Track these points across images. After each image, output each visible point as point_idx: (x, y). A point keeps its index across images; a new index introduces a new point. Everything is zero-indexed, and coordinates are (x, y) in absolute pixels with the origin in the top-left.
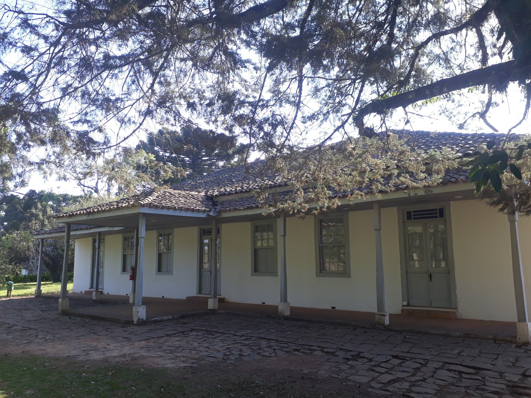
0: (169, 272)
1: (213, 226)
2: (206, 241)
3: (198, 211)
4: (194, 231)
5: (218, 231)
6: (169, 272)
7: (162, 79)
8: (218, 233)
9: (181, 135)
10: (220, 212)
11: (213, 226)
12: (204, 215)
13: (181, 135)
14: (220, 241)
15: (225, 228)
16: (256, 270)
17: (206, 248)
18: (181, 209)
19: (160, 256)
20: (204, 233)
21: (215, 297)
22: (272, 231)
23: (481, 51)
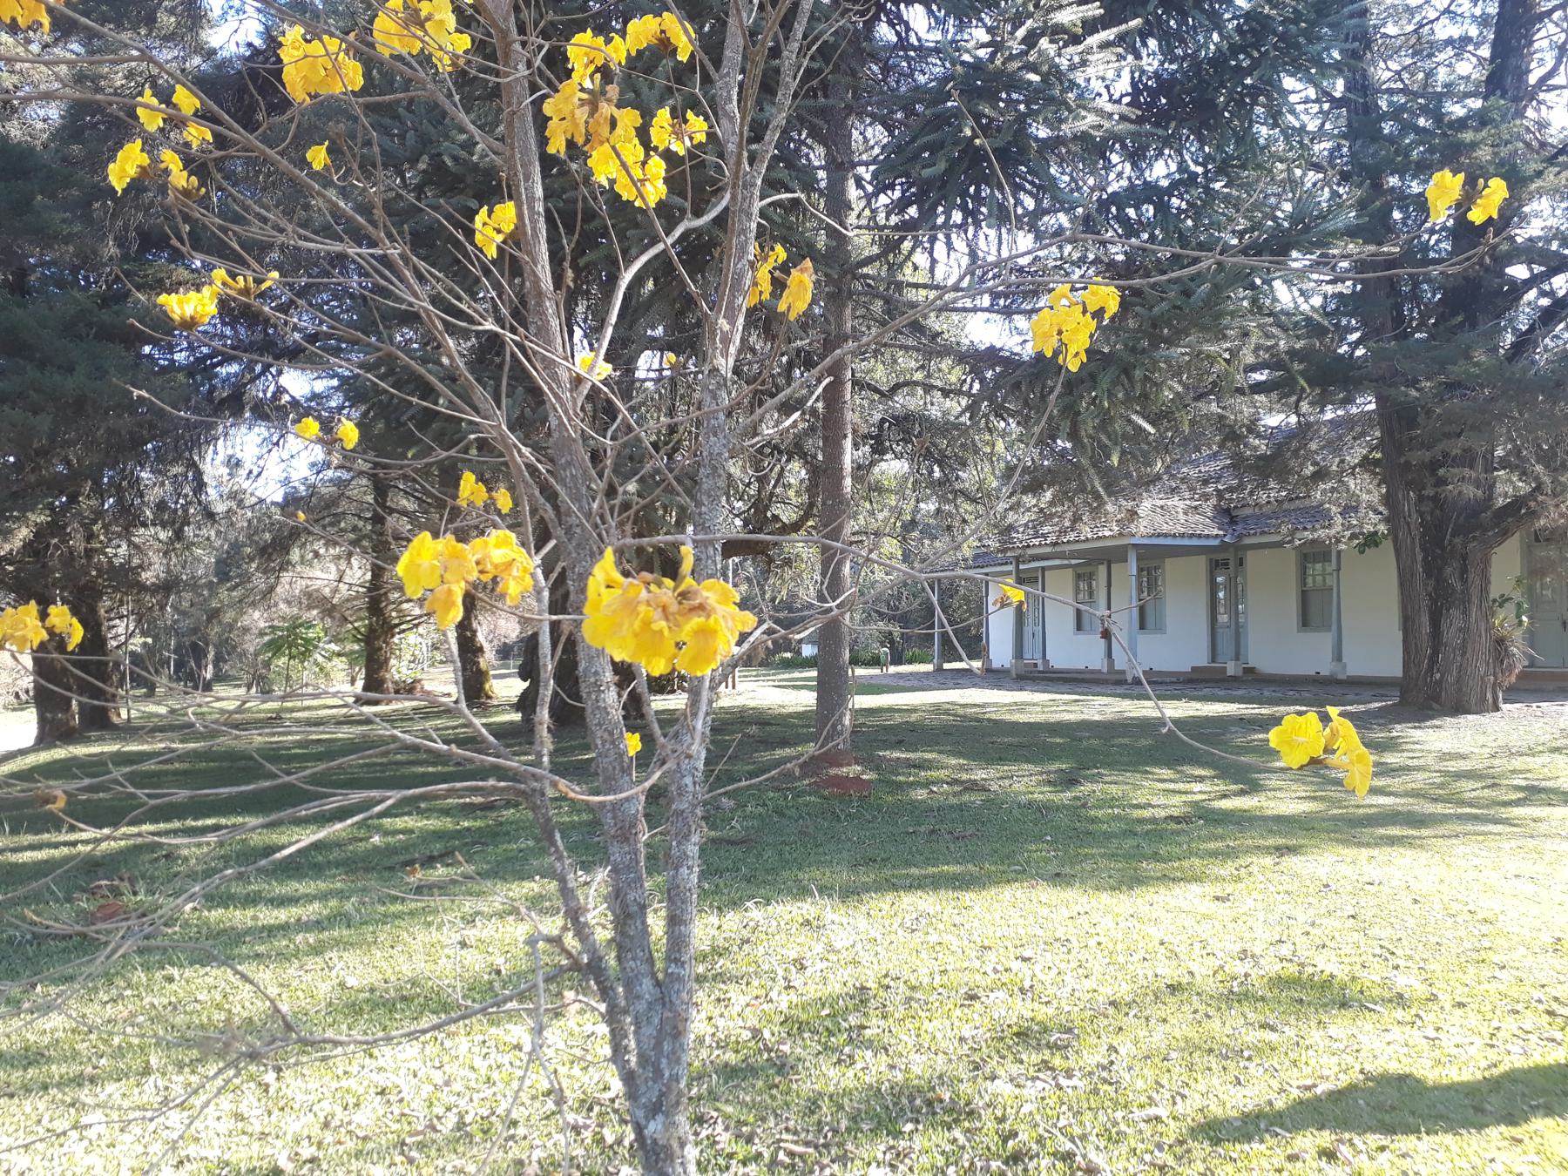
0: (1160, 629)
1: (1230, 555)
2: (1219, 579)
3: (1208, 536)
4: (1201, 562)
5: (1241, 562)
6: (1160, 629)
7: (1179, 52)
8: (1241, 564)
9: (1151, 59)
10: (1240, 537)
11: (1230, 555)
12: (1216, 542)
13: (1151, 59)
14: (1245, 578)
15: (1250, 556)
16: (1305, 622)
17: (1221, 595)
18: (1182, 536)
19: (1142, 610)
20: (1216, 565)
21: (1237, 659)
22: (1403, 702)
23: (1526, 209)
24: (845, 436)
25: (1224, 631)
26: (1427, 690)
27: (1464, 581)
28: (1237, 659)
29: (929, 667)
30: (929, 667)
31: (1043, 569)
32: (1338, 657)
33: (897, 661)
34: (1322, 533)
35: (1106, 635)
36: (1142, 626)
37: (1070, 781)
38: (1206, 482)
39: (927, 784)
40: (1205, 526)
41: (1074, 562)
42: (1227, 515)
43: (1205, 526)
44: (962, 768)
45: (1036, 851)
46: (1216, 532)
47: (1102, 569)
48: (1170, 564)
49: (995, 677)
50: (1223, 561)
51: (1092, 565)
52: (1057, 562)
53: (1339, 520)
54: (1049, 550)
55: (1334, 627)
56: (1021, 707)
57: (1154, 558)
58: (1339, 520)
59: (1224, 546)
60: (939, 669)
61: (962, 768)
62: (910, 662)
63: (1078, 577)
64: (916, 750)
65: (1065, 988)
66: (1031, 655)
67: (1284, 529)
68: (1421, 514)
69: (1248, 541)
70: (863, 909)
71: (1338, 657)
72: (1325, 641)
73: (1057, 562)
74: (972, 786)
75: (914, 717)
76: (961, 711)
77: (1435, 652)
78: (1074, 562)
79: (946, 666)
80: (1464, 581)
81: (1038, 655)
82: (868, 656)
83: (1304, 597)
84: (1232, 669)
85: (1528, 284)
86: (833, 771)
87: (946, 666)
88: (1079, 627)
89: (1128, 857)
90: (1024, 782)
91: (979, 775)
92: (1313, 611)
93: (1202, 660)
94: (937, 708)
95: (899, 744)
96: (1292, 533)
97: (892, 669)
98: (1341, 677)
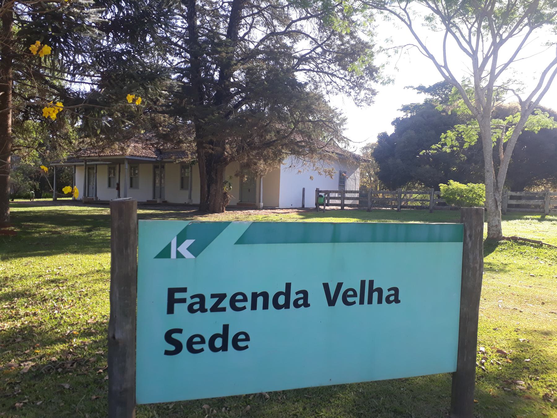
0: (137, 187)
3: (152, 158)
4: (151, 166)
6: (137, 187)
10: (162, 159)
12: (154, 160)
16: (182, 187)
20: (155, 167)
21: (160, 197)
24: (9, 113)
25: (157, 190)
26: (206, 208)
27: (216, 176)
28: (160, 197)
29: (51, 199)
30: (51, 199)
31: (96, 165)
32: (190, 198)
33: (37, 197)
34: (185, 160)
35: (118, 189)
36: (131, 186)
37: (89, 230)
38: (147, 140)
39: (39, 232)
40: (151, 153)
41: (107, 163)
42: (159, 152)
43: (151, 153)
44: (53, 228)
45: (71, 247)
46: (155, 156)
47: (118, 166)
48: (141, 166)
49: (75, 202)
50: (158, 166)
51: (115, 164)
52: (102, 162)
53: (190, 156)
54: (97, 158)
55: (189, 188)
56: (81, 211)
57: (135, 163)
58: (190, 156)
59: (157, 161)
60: (55, 200)
61: (53, 228)
62: (45, 198)
63: (109, 168)
64: (36, 222)
65: (67, 272)
66: (92, 196)
67: (173, 157)
68: (206, 156)
69: (165, 160)
70: (9, 262)
71: (190, 198)
72: (187, 192)
73: (102, 162)
74: (56, 233)
75: (38, 214)
76: (59, 212)
77: (208, 196)
78: (107, 163)
79: (58, 199)
80: (216, 176)
81: (94, 195)
82: (24, 194)
83: (182, 179)
84: (159, 201)
85: (236, 94)
86: (2, 229)
87: (58, 199)
88: (109, 186)
89: (100, 247)
90: (75, 231)
91: (59, 229)
92: (184, 184)
93: (150, 198)
94: (50, 211)
95: (30, 221)
96: (175, 159)
97: (35, 200)
98: (191, 204)
